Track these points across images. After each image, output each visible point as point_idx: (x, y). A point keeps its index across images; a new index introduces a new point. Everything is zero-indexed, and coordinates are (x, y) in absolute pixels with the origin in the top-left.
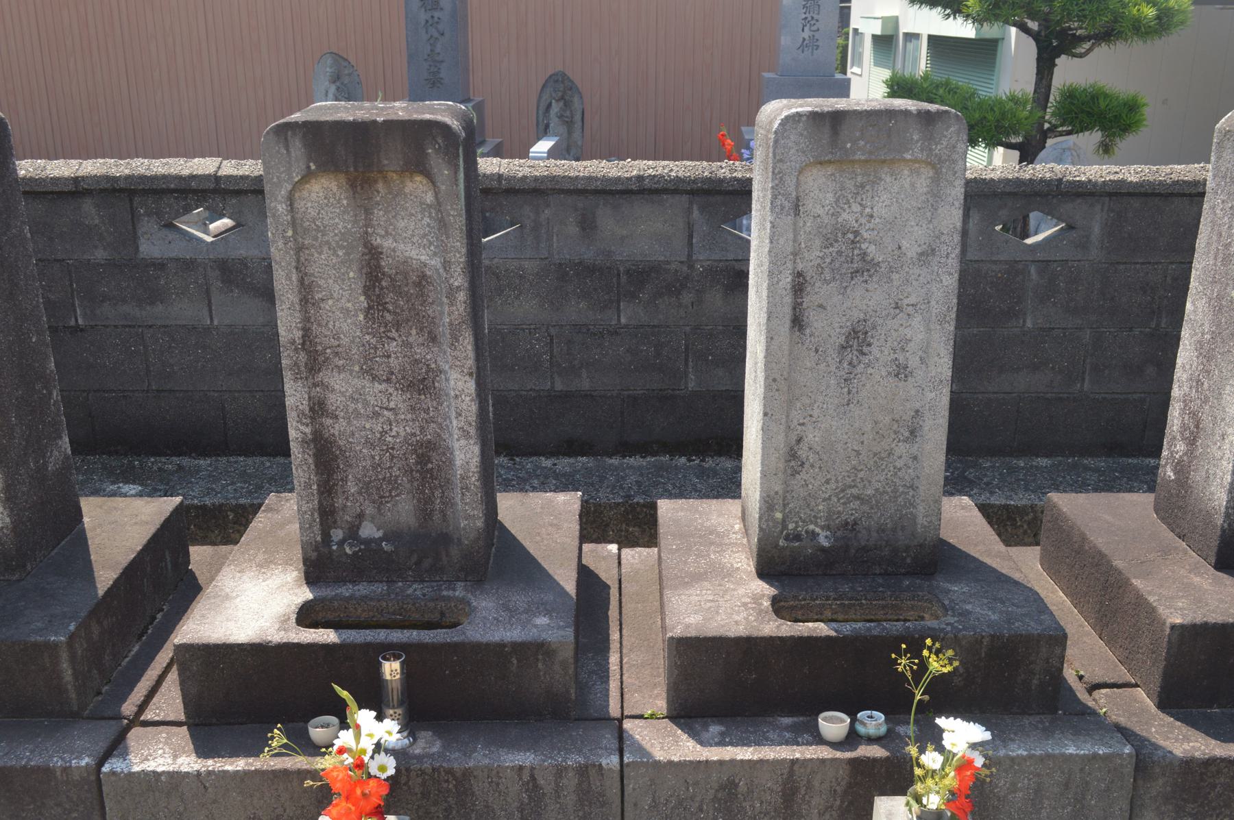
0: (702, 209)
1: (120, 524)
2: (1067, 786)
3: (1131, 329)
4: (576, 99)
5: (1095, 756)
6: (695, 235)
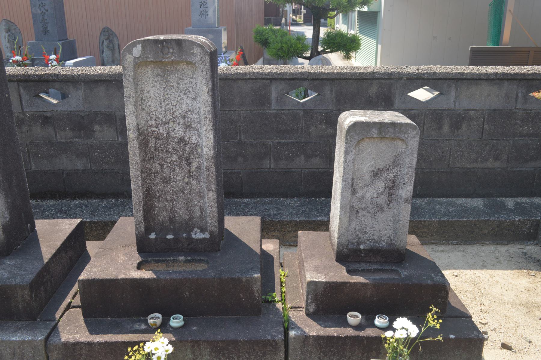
0: (24, 88)
1: (53, 232)
2: (14, 354)
3: (228, 141)
4: (115, 39)
5: (24, 342)
6: (23, 100)
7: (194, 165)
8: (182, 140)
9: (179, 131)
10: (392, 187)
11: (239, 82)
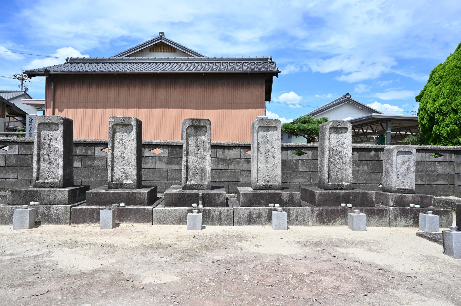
7: (344, 160)
8: (341, 152)
9: (340, 149)
10: (408, 167)
11: (189, 165)
